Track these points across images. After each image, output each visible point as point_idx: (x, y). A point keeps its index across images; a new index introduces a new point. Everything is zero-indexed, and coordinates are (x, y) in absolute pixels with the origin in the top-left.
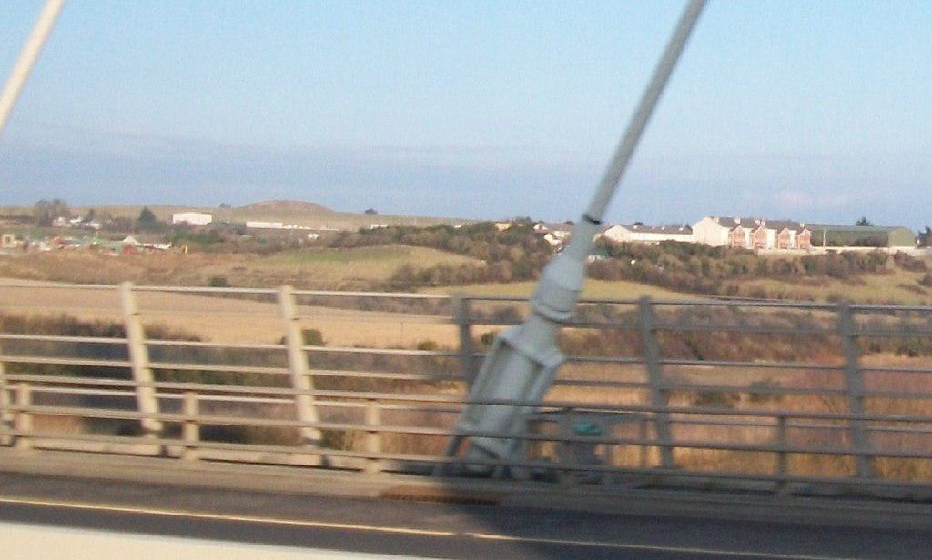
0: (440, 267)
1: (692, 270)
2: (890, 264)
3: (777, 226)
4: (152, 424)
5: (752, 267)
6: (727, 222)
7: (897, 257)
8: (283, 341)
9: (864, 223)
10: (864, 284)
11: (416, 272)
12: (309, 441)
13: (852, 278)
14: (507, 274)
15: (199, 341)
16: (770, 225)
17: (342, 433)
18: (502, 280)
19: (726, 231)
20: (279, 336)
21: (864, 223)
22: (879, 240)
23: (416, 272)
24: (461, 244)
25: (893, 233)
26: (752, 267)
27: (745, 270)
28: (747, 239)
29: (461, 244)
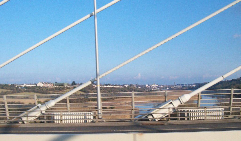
0: (7, 91)
1: (41, 90)
2: (65, 88)
3: (49, 83)
4: (8, 118)
5: (49, 89)
6: (42, 83)
7: (66, 87)
8: (35, 103)
9: (56, 82)
10: (64, 91)
11: (4, 92)
12: (8, 119)
13: (62, 90)
14: (16, 92)
15: (24, 104)
16: (48, 83)
17: (177, 118)
18: (15, 93)
19: (43, 84)
20: (34, 103)
21: (56, 82)
22: (63, 84)
23: (4, 92)
24: (5, 88)
25: (65, 83)
26: (49, 89)
27: (48, 90)
28: (45, 86)
29: (5, 88)
